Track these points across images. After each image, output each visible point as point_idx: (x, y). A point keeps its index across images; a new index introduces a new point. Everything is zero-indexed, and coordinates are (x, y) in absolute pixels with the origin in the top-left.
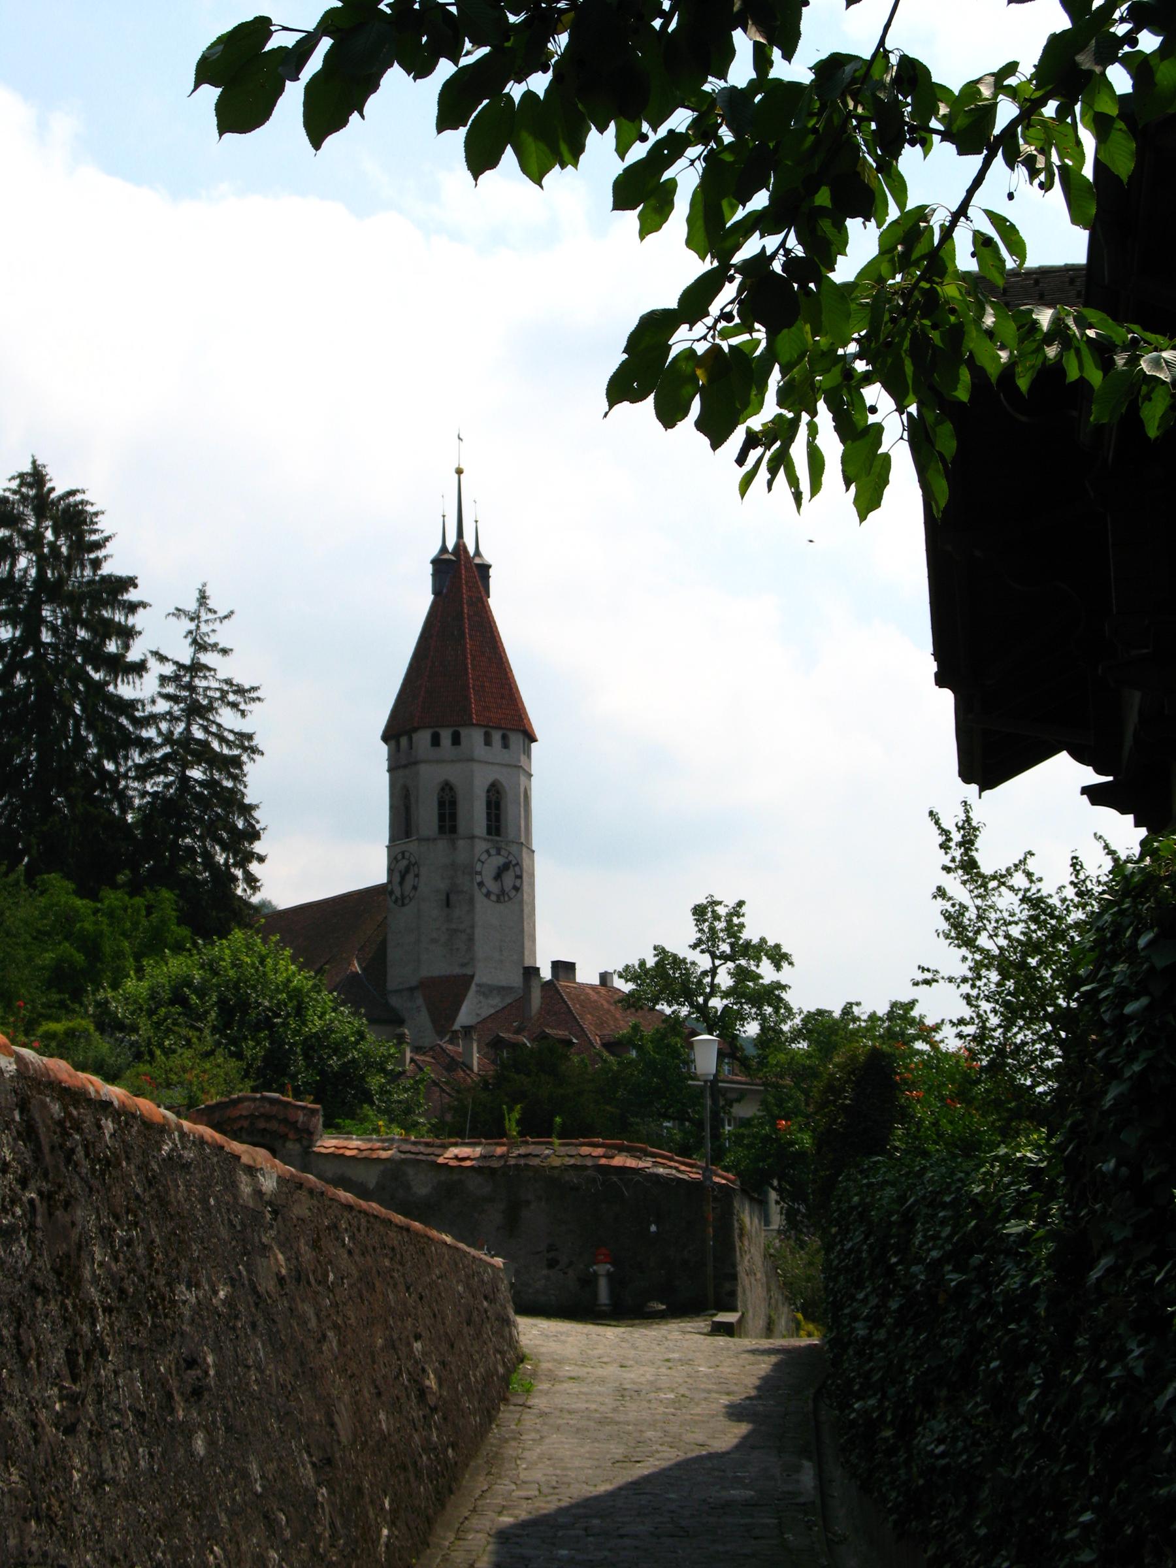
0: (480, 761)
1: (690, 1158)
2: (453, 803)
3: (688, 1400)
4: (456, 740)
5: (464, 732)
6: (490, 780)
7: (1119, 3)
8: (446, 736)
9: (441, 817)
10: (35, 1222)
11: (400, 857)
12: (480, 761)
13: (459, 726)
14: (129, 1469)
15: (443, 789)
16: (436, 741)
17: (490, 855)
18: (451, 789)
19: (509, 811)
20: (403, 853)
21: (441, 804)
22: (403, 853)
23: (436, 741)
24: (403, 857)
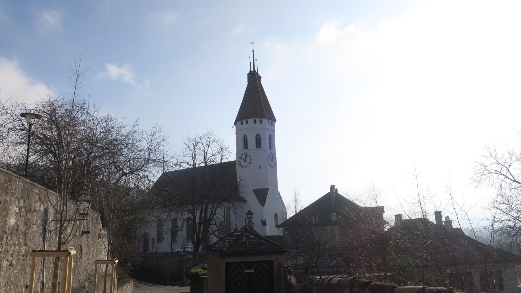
0: (242, 159)
1: (90, 208)
2: (260, 140)
3: (480, 181)
4: (261, 122)
5: (263, 120)
6: (269, 134)
7: (103, 292)
8: (258, 120)
9: (257, 143)
10: (186, 248)
11: (243, 154)
12: (242, 159)
13: (261, 118)
14: (122, 234)
15: (257, 136)
16: (255, 122)
17: (245, 166)
18: (259, 136)
19: (271, 141)
20: (245, 153)
21: (256, 140)
22: (245, 153)
23: (255, 122)
24: (245, 154)
